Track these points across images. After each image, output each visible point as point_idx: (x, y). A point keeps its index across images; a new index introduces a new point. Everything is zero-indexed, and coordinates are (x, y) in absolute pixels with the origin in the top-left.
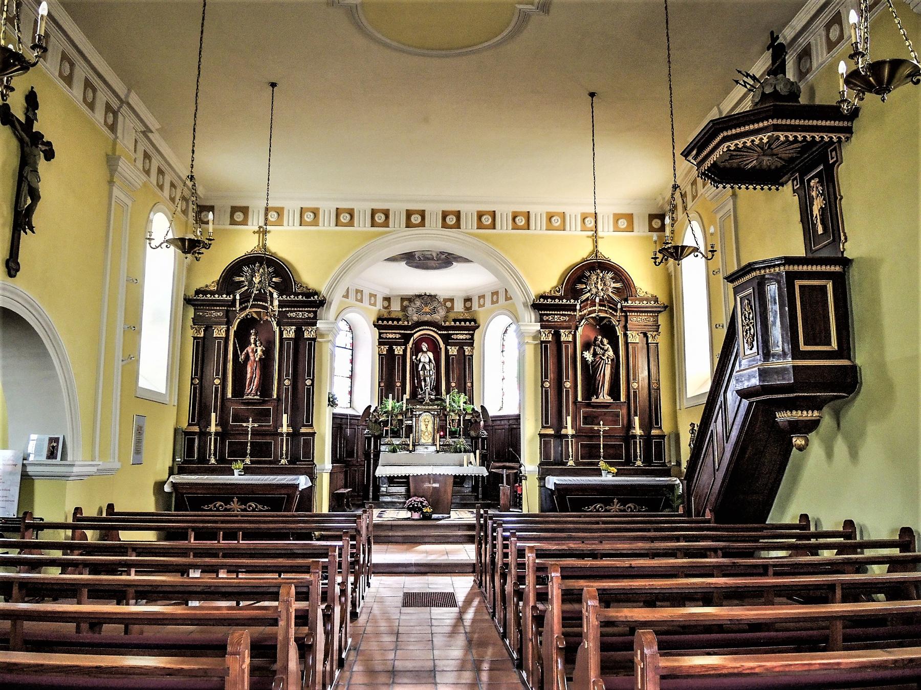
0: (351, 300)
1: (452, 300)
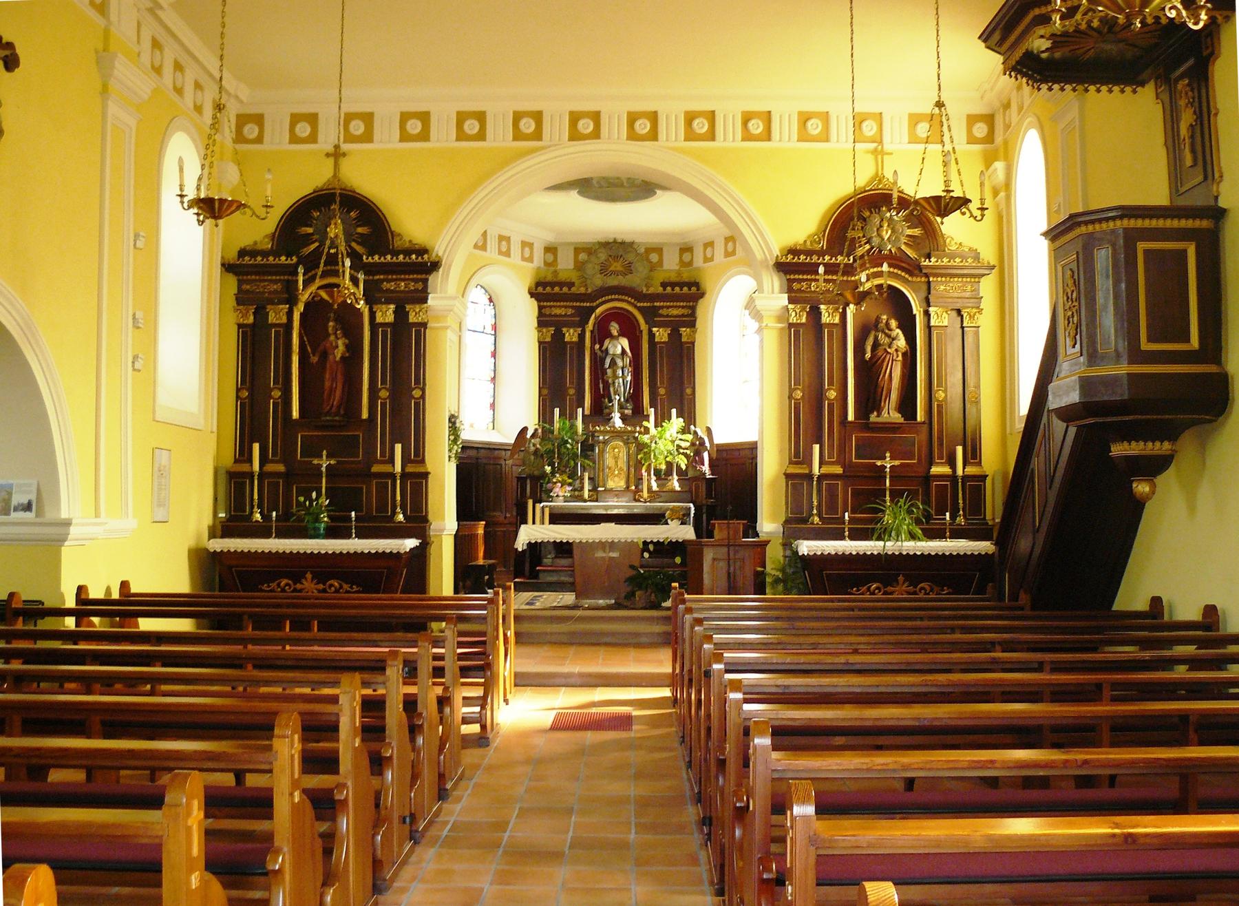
0: (492, 251)
1: (659, 250)
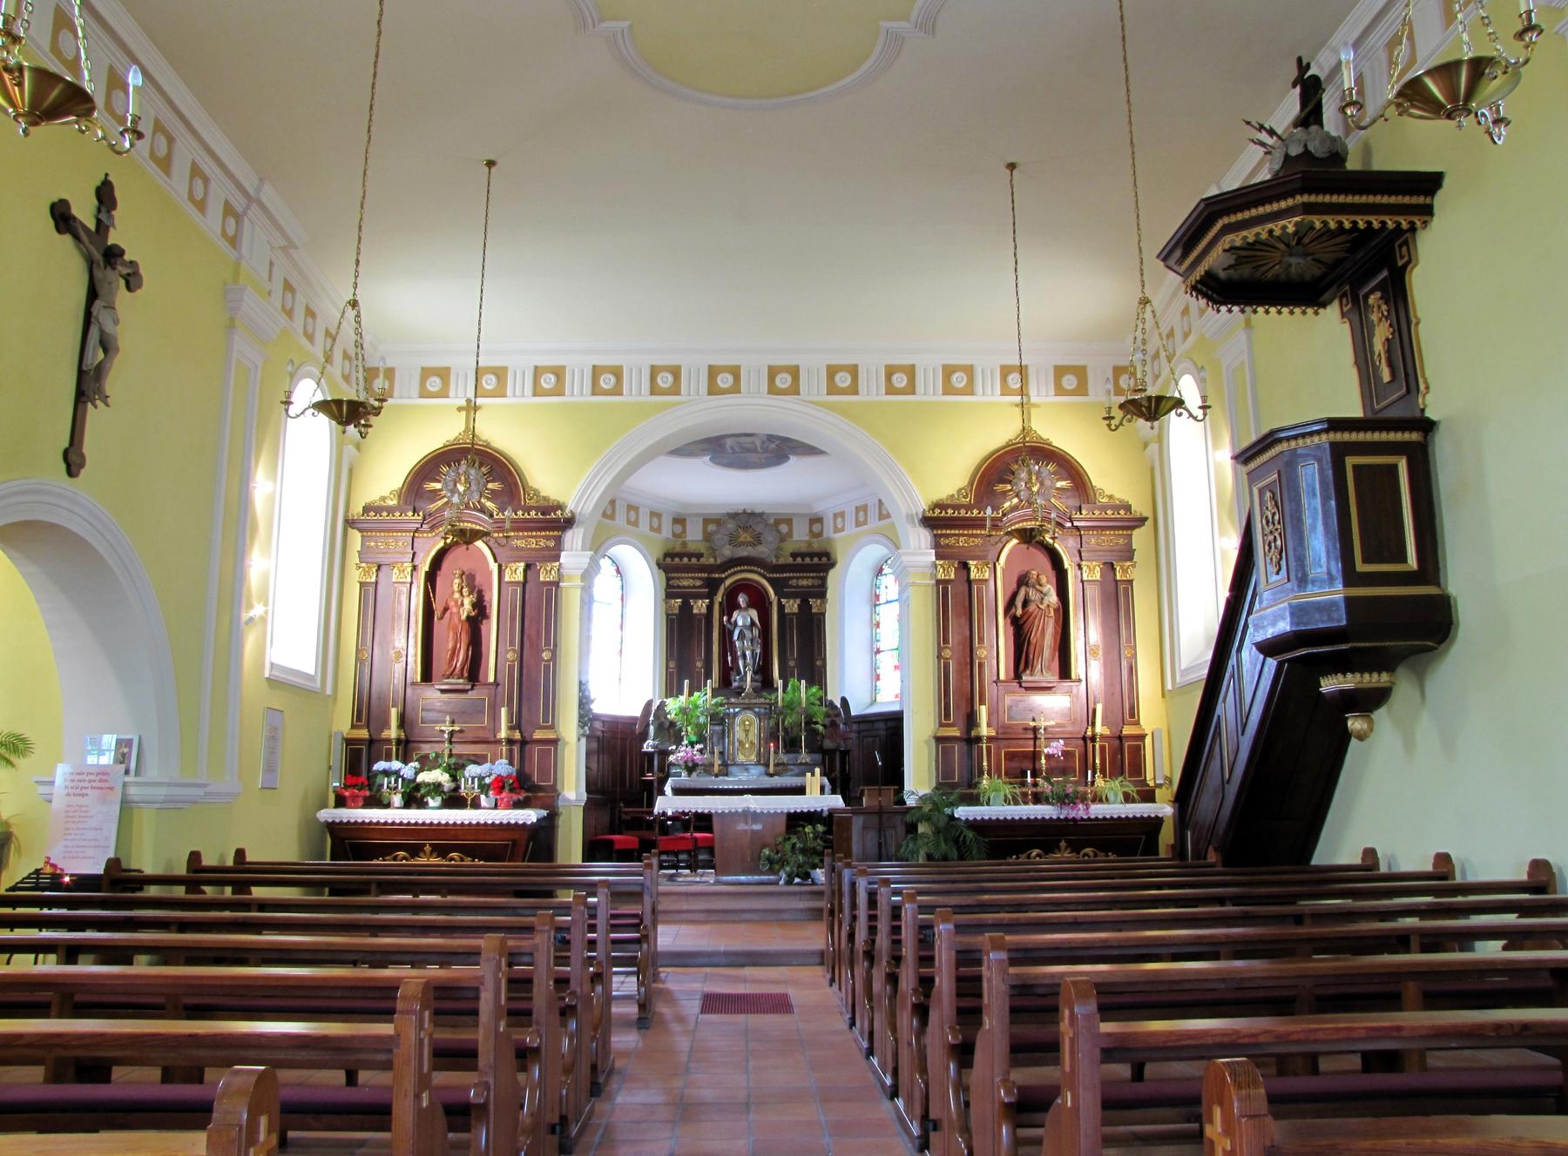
1: (789, 521)
